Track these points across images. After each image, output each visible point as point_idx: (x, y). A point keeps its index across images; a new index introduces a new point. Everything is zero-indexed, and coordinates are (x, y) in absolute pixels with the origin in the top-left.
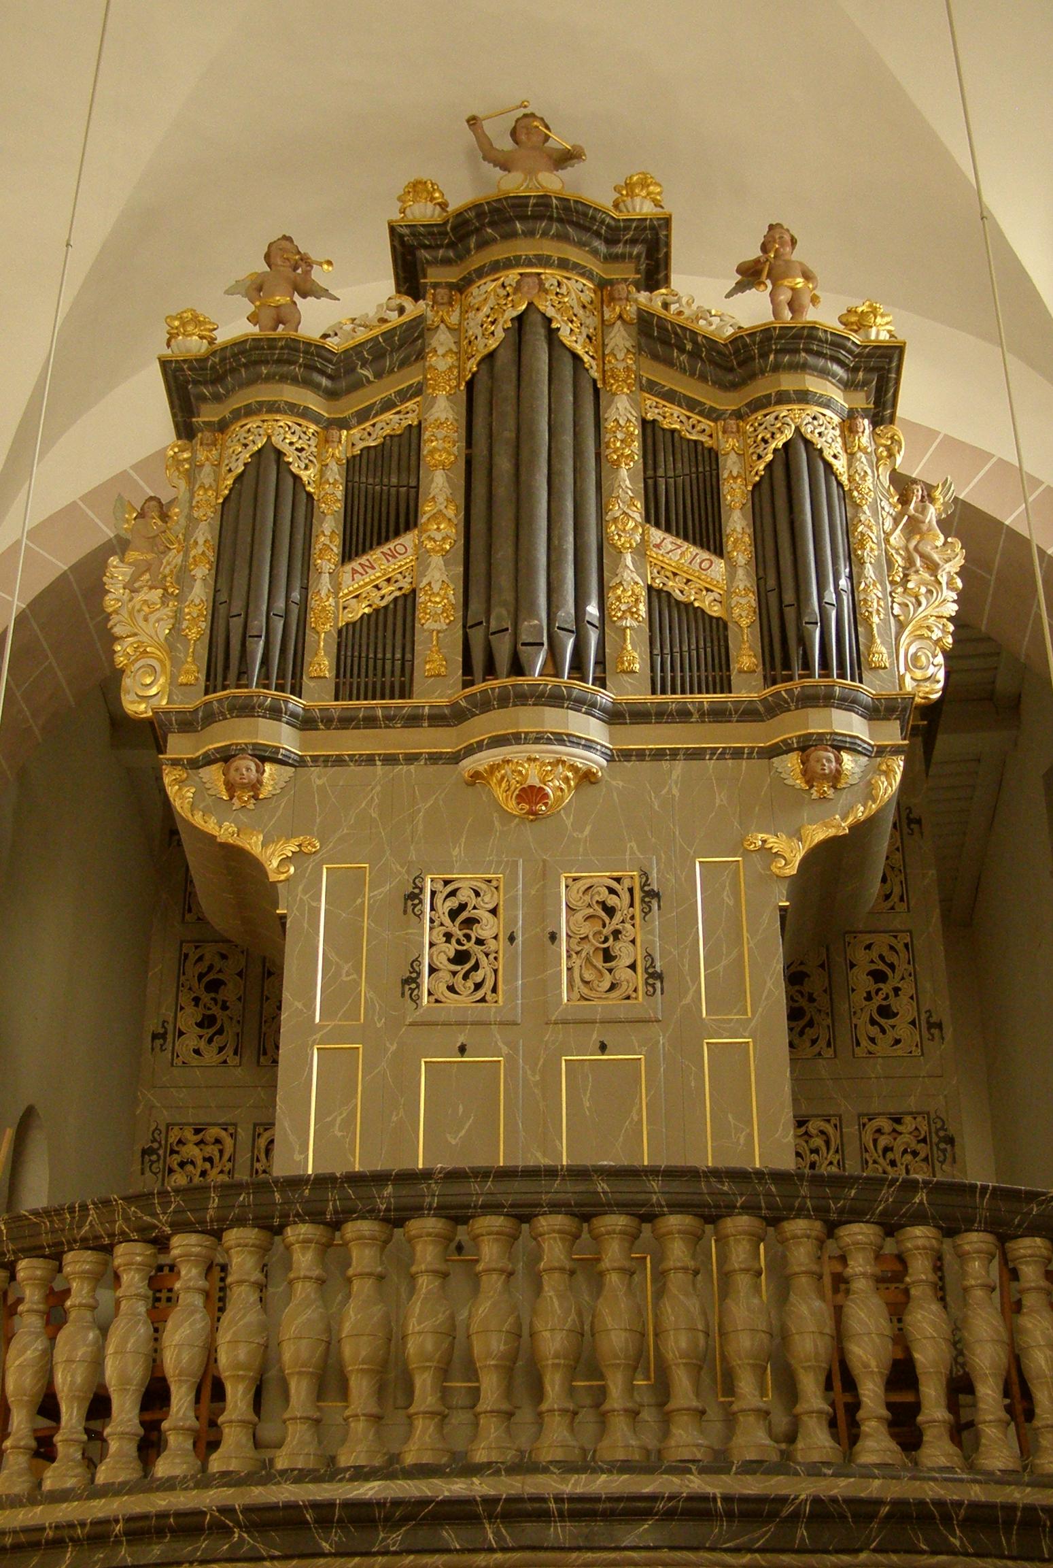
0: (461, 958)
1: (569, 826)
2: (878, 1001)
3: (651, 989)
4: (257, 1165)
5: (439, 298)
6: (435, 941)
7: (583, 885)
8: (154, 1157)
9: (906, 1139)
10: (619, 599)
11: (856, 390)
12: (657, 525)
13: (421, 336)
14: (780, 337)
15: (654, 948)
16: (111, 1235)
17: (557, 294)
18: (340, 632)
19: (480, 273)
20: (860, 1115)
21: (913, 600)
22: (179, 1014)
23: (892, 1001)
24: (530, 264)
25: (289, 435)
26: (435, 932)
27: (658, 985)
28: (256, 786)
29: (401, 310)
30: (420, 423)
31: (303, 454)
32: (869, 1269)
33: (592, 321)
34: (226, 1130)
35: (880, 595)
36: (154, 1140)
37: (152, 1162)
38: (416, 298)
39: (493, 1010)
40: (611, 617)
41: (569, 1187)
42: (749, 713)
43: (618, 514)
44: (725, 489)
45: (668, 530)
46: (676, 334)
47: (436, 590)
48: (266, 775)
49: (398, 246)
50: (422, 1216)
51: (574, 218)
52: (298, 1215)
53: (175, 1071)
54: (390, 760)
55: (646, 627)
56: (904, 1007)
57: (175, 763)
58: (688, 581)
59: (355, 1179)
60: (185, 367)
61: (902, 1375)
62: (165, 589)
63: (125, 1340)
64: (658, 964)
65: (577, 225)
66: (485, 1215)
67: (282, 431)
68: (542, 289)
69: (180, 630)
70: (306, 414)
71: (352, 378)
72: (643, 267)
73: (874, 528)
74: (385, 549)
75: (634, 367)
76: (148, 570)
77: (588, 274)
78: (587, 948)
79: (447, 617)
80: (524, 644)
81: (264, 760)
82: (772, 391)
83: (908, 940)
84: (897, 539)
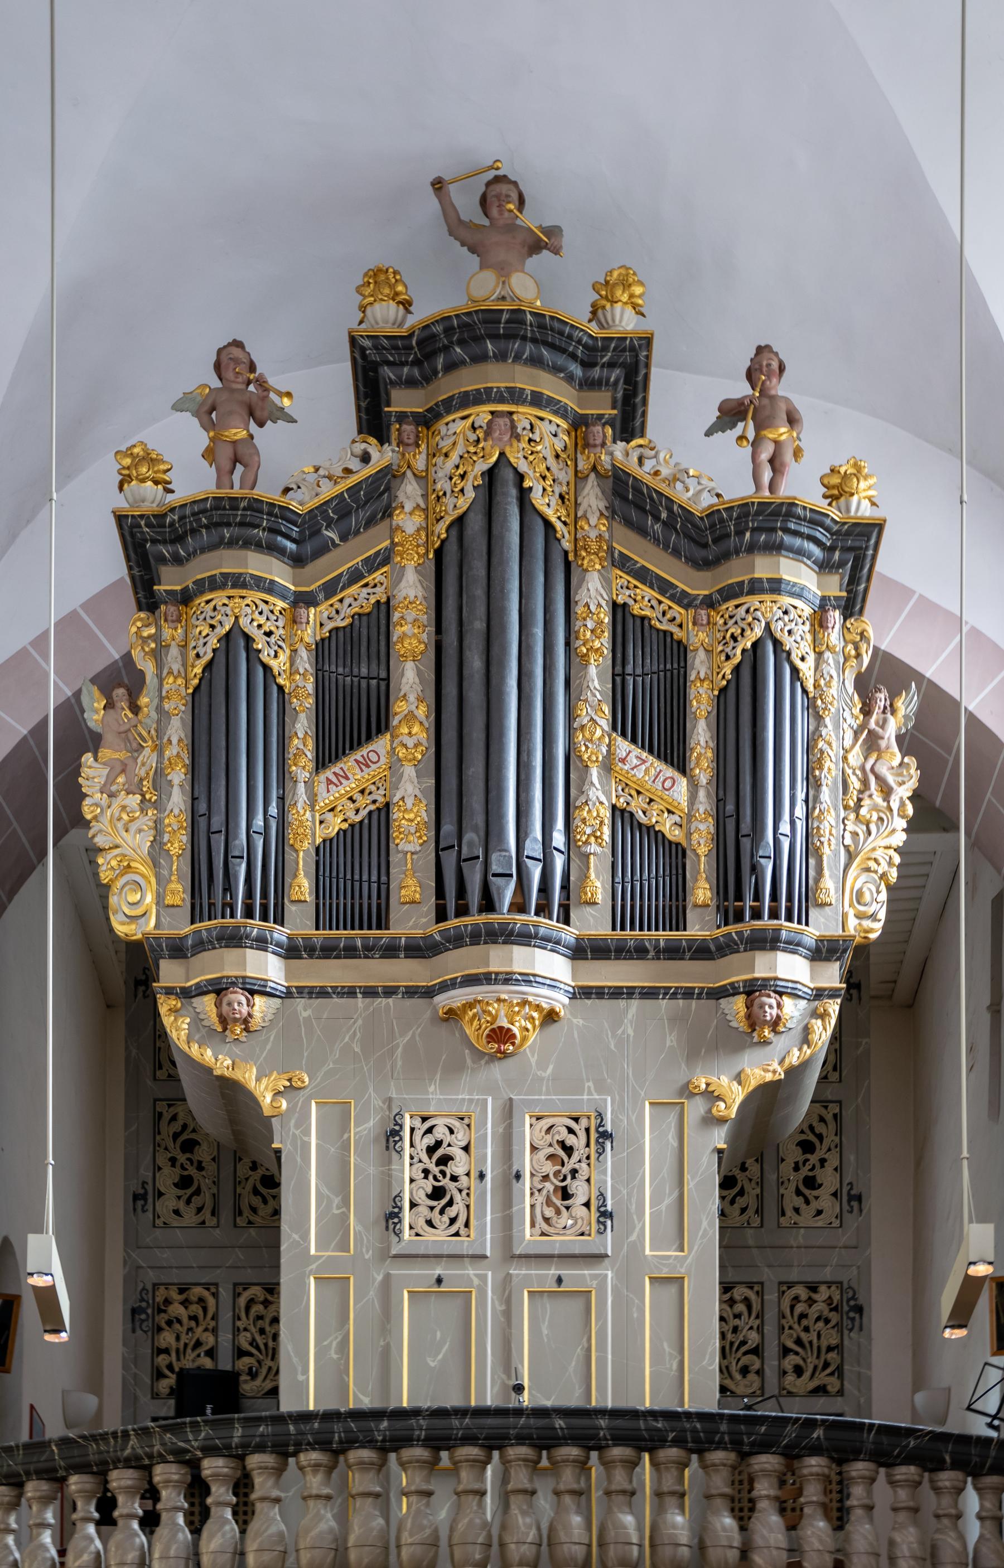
0: (437, 1193)
1: (534, 1064)
2: (804, 1171)
3: (602, 1227)
4: (239, 1323)
5: (405, 436)
6: (415, 1177)
7: (545, 1124)
8: (143, 1316)
10: (584, 821)
11: (830, 572)
12: (624, 734)
13: (388, 489)
14: (758, 513)
15: (606, 1189)
16: (150, 1456)
17: (530, 440)
18: (317, 849)
19: (449, 405)
20: (780, 1283)
21: (864, 828)
22: (157, 1175)
23: (818, 1172)
24: (502, 400)
25: (256, 615)
26: (415, 1167)
27: (609, 1223)
29: (365, 458)
30: (388, 599)
31: (272, 640)
32: (772, 1492)
33: (565, 475)
34: (208, 1289)
35: (833, 823)
36: (142, 1300)
37: (143, 1321)
38: (383, 439)
39: (466, 1244)
40: (576, 841)
41: (532, 1421)
42: (702, 951)
43: (585, 721)
44: (692, 692)
45: (634, 741)
46: (652, 499)
47: (409, 805)
48: (256, 1008)
49: (359, 360)
50: (412, 1446)
52: (309, 1444)
53: (158, 1231)
54: (370, 992)
55: (608, 851)
56: (828, 1179)
57: (169, 991)
58: (651, 800)
59: (357, 1415)
60: (143, 523)
62: (143, 796)
63: (167, 1548)
64: (609, 1203)
65: (552, 346)
66: (463, 1445)
67: (249, 610)
69: (162, 844)
72: (620, 395)
73: (834, 745)
74: (358, 755)
75: (607, 536)
76: (123, 771)
77: (562, 411)
78: (549, 1187)
79: (420, 837)
80: (494, 875)
81: (252, 992)
83: (837, 1110)
84: (855, 757)
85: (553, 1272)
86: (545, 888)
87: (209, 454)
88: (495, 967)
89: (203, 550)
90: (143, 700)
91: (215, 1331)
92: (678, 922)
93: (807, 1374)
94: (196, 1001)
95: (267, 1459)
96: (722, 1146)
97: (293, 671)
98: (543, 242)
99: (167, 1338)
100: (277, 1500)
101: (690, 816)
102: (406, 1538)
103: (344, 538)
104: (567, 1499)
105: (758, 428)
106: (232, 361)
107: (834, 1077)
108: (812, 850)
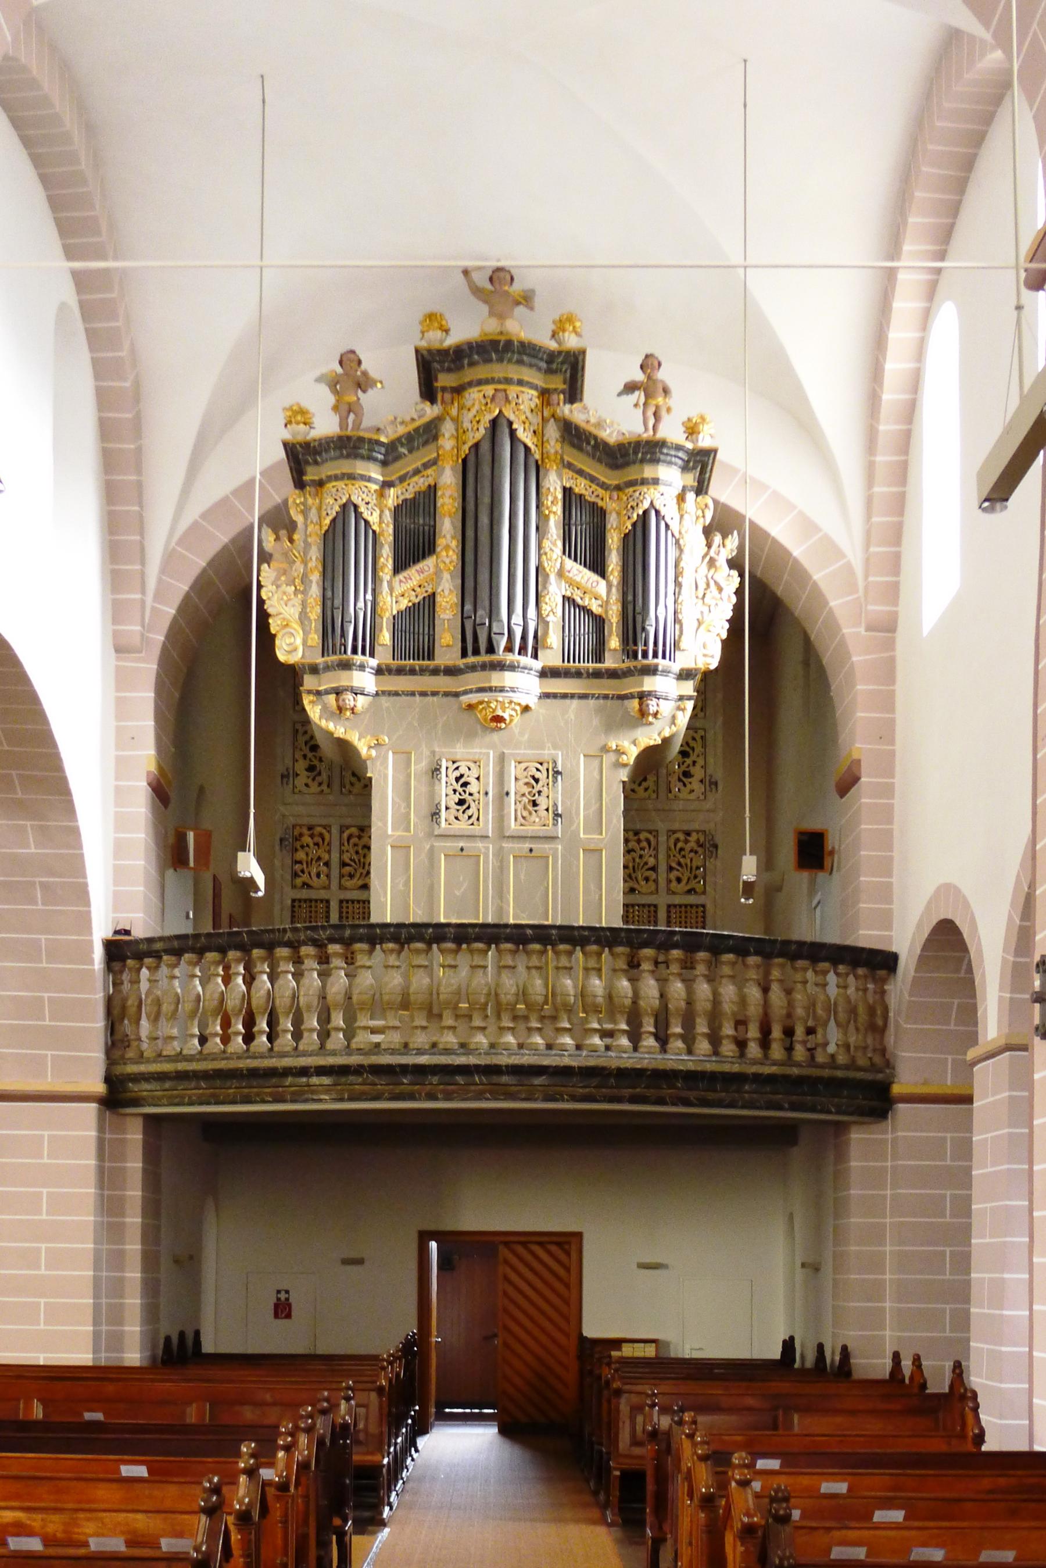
0: (461, 802)
7: (523, 766)
9: (692, 844)
19: (470, 384)
24: (499, 382)
25: (363, 495)
31: (370, 506)
33: (536, 420)
42: (613, 674)
44: (608, 536)
45: (575, 560)
54: (423, 694)
56: (698, 772)
57: (309, 692)
59: (414, 925)
65: (529, 355)
68: (507, 400)
69: (306, 613)
71: (395, 454)
77: (534, 387)
82: (639, 477)
85: (527, 845)
86: (524, 638)
87: (336, 408)
88: (494, 683)
89: (332, 459)
90: (296, 537)
91: (329, 852)
92: (599, 657)
93: (684, 882)
94: (324, 697)
95: (365, 946)
96: (626, 779)
97: (381, 522)
98: (526, 299)
99: (301, 855)
100: (369, 967)
101: (607, 602)
102: (442, 989)
103: (410, 451)
104: (534, 971)
105: (647, 396)
106: (349, 360)
107: (701, 715)
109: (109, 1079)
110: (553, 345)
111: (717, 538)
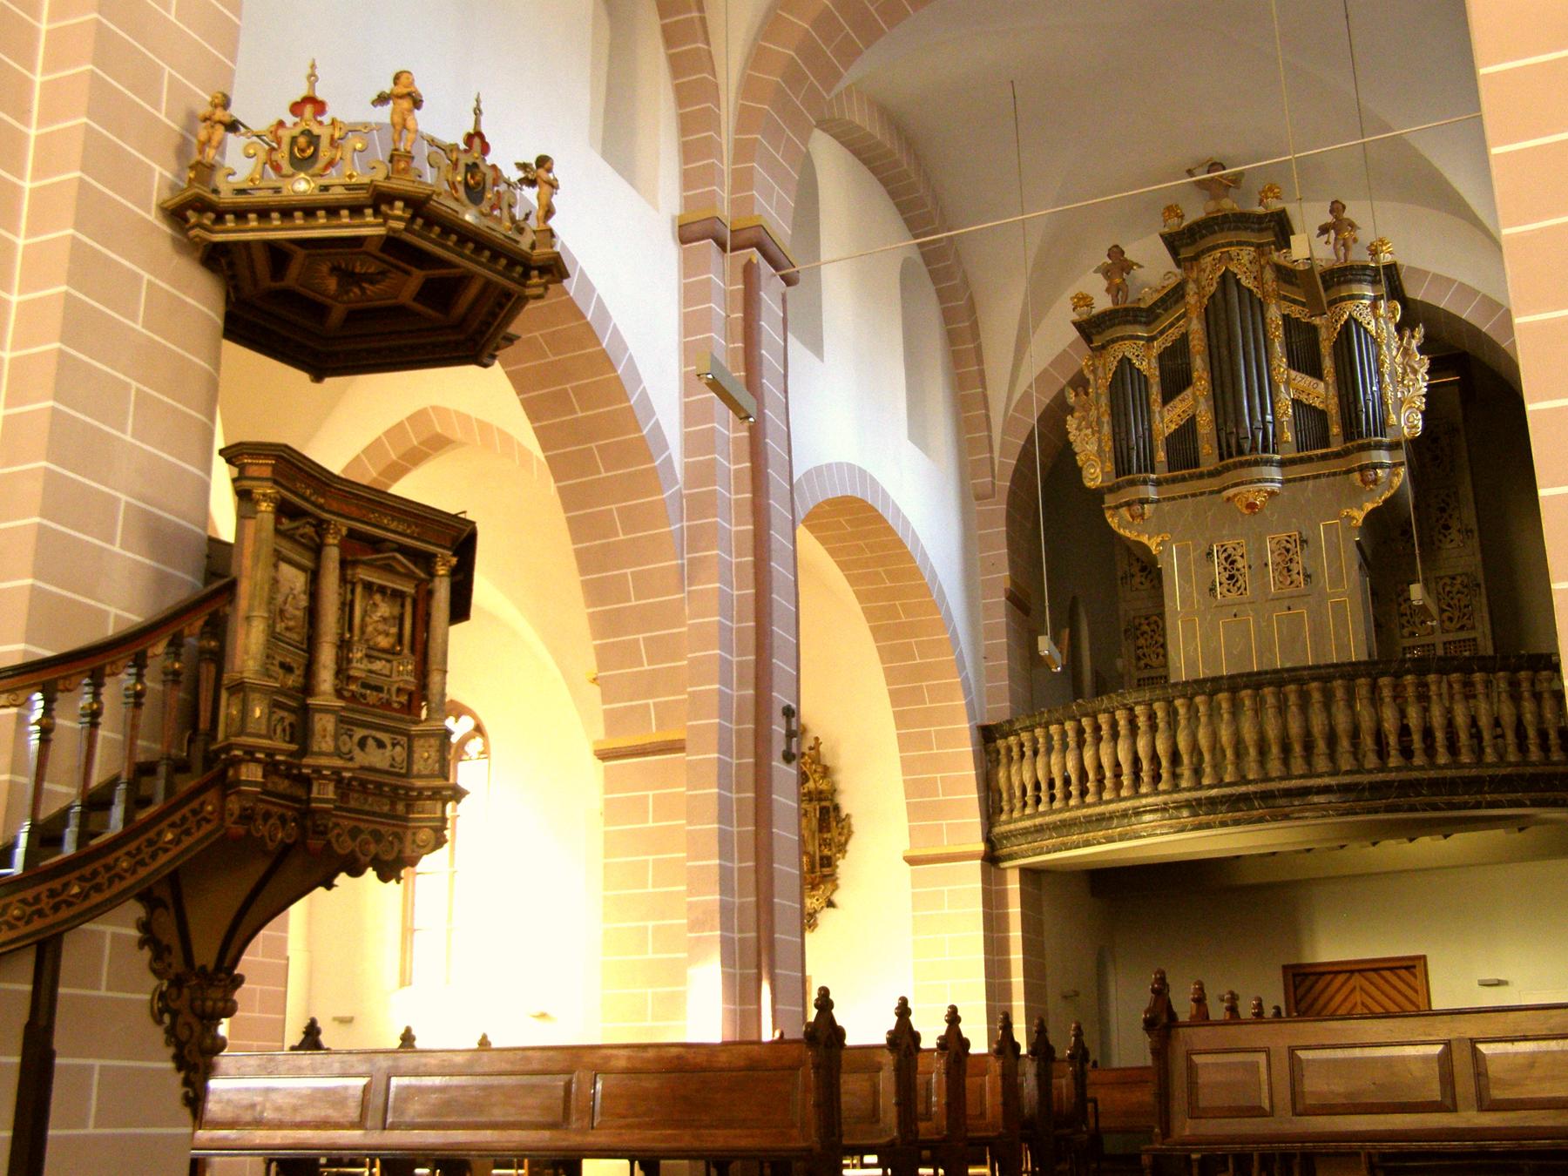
0: (1231, 577)
19: (1203, 252)
25: (1128, 349)
28: (1142, 515)
33: (1255, 268)
42: (1337, 455)
51: (1242, 221)
54: (1194, 495)
61: (1404, 731)
70: (1138, 338)
84: (1399, 359)
99: (1141, 642)
106: (1116, 252)
108: (1383, 402)
109: (988, 840)
110: (1260, 210)
111: (1407, 333)
